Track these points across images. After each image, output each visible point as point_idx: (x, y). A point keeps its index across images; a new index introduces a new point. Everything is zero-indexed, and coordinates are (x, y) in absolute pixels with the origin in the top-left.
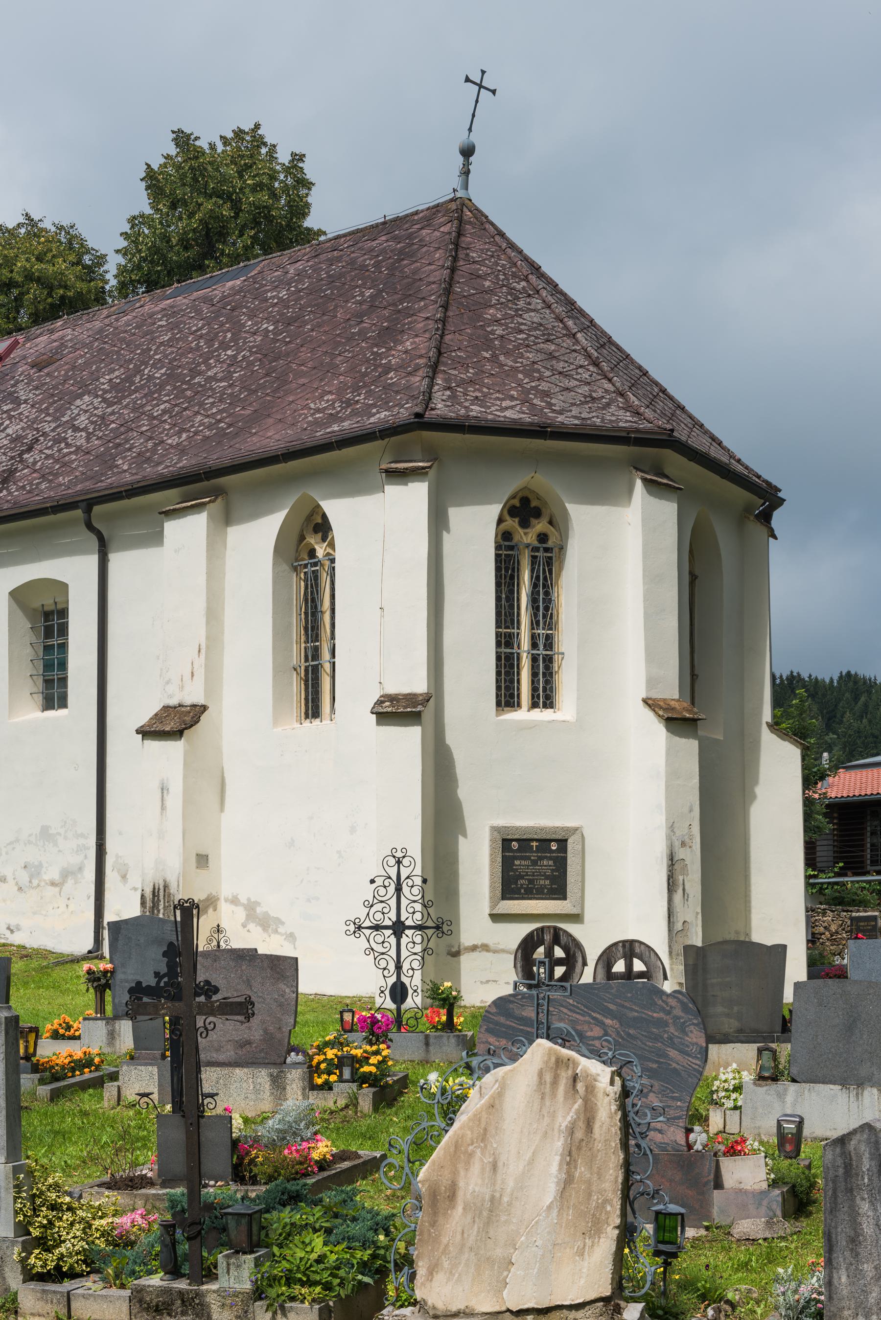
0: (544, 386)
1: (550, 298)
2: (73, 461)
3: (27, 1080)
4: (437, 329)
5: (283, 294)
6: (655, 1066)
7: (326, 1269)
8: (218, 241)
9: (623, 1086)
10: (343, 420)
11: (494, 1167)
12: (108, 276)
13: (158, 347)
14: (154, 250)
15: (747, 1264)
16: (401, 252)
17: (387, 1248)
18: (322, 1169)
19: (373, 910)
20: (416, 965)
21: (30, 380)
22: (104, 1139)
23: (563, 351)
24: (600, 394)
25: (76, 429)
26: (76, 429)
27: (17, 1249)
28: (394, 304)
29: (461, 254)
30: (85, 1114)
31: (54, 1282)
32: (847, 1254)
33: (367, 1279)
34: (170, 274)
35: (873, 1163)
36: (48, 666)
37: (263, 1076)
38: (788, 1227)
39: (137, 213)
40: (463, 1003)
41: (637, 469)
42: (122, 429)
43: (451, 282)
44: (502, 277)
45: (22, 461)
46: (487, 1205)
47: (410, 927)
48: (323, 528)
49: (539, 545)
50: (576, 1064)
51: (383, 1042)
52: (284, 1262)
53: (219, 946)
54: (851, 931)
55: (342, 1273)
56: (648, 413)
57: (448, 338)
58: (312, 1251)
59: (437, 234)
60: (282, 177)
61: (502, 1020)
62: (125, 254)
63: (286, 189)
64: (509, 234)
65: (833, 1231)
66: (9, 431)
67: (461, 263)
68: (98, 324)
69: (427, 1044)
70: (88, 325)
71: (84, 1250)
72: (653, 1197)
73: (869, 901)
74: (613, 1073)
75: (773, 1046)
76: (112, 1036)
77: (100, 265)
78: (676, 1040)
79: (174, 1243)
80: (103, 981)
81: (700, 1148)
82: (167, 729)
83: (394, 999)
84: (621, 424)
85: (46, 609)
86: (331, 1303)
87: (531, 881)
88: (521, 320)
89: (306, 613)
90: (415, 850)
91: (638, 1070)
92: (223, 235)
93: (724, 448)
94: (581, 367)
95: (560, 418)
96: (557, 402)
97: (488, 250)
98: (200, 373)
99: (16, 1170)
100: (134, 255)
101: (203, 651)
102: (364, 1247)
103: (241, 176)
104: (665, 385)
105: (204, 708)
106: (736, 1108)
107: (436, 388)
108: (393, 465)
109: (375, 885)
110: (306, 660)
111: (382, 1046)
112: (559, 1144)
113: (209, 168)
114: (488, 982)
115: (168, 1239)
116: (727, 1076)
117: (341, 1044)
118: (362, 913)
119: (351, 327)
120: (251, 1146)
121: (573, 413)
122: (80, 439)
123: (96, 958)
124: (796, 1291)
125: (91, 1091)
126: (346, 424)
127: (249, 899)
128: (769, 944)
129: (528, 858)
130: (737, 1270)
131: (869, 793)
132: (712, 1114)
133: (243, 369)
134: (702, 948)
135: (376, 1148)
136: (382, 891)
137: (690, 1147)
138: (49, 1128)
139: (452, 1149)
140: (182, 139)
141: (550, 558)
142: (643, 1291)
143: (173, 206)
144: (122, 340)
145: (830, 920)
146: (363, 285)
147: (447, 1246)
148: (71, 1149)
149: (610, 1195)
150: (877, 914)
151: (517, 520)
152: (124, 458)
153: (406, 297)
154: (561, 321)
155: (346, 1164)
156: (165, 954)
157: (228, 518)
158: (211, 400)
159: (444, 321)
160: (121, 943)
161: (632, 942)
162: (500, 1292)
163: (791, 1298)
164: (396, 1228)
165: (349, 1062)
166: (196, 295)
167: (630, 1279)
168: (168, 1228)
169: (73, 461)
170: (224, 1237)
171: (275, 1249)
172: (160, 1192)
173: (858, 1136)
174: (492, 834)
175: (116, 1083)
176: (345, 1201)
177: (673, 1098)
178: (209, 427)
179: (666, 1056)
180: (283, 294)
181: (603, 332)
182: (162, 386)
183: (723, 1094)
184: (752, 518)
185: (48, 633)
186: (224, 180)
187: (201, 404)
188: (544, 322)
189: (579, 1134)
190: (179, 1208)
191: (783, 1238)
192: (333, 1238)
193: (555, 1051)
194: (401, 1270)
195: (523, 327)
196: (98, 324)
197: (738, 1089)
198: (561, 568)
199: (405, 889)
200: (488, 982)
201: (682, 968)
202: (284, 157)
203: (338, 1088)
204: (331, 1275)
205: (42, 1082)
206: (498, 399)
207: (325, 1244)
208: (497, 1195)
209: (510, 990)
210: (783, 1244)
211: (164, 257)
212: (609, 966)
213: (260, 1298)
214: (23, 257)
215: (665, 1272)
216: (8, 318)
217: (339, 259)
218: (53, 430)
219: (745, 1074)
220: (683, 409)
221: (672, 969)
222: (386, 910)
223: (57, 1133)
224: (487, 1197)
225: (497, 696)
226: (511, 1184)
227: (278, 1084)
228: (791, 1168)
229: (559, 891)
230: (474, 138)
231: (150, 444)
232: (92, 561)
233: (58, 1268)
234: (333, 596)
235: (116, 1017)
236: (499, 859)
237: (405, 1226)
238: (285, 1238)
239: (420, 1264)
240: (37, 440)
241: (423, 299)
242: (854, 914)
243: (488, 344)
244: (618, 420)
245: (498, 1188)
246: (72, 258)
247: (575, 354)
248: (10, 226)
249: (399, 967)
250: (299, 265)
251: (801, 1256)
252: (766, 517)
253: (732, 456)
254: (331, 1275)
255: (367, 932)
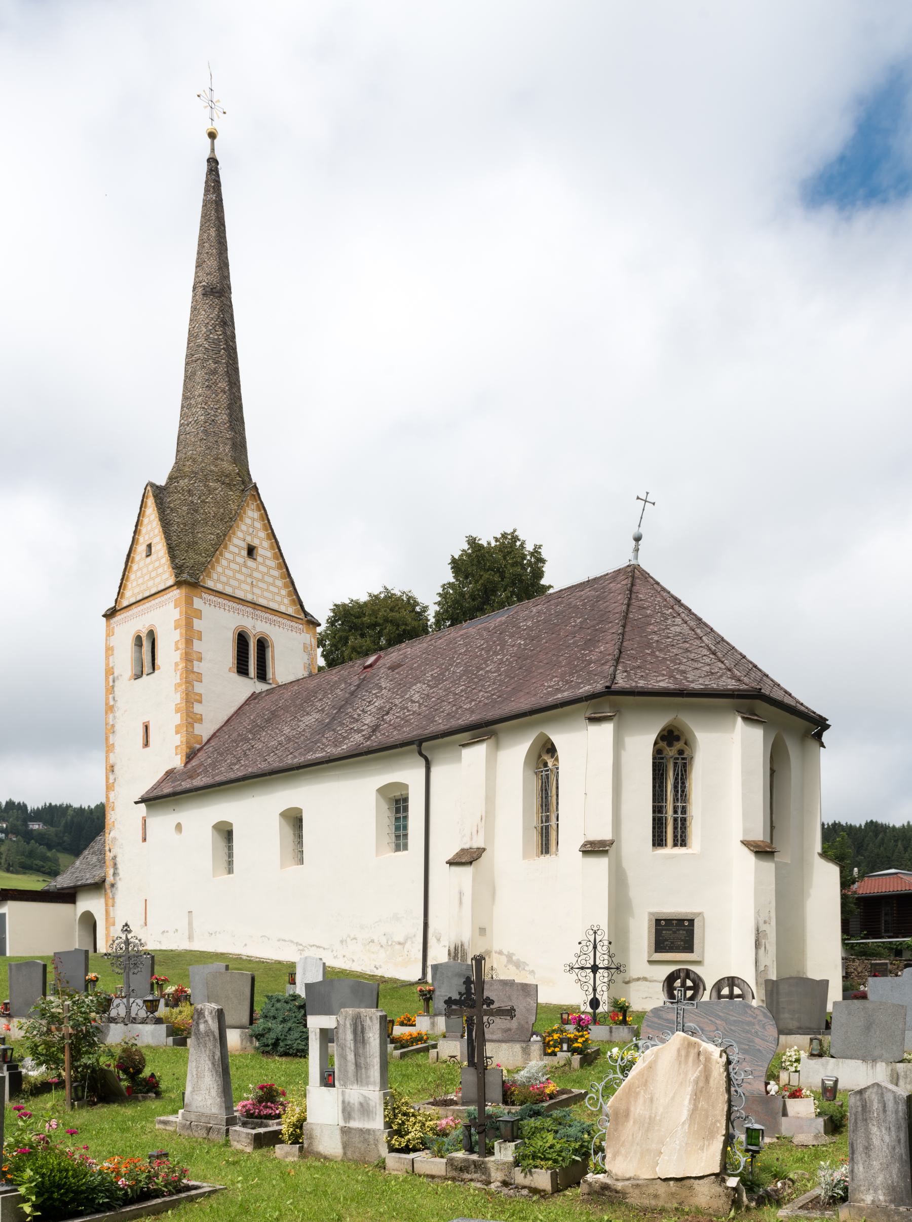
0: (682, 667)
1: (686, 618)
2: (411, 719)
3: (390, 1047)
4: (619, 639)
5: (529, 623)
6: (747, 1047)
7: (555, 1152)
8: (492, 595)
9: (728, 1058)
10: (564, 691)
11: (652, 1100)
12: (429, 617)
13: (459, 656)
14: (456, 602)
15: (802, 1159)
16: (597, 597)
17: (589, 1142)
18: (551, 1098)
19: (580, 958)
20: (605, 988)
21: (387, 675)
22: (430, 1079)
23: (694, 647)
24: (717, 670)
25: (413, 702)
26: (413, 702)
27: (386, 1135)
28: (594, 626)
29: (634, 596)
30: (419, 1066)
31: (405, 1153)
32: (863, 1155)
33: (578, 1158)
34: (464, 614)
35: (880, 1105)
36: (397, 828)
37: (517, 1047)
38: (827, 1139)
39: (446, 582)
40: (631, 1010)
41: (738, 712)
42: (439, 701)
43: (627, 612)
44: (657, 607)
45: (383, 720)
46: (647, 1121)
47: (601, 968)
48: (551, 750)
49: (678, 756)
50: (699, 1046)
51: (586, 1031)
52: (531, 1147)
53: (492, 978)
54: (871, 971)
55: (563, 1154)
56: (746, 680)
57: (625, 644)
58: (547, 1142)
59: (619, 586)
60: (528, 558)
61: (656, 1020)
62: (439, 605)
63: (530, 564)
64: (662, 583)
65: (854, 1142)
66: (376, 704)
67: (634, 601)
68: (425, 645)
69: (611, 1032)
70: (420, 646)
71: (421, 1137)
72: (745, 1120)
73: (883, 954)
74: (721, 1051)
75: (820, 1037)
76: (433, 1024)
77: (425, 611)
78: (759, 1033)
79: (470, 1135)
80: (428, 996)
81: (774, 1093)
82: (463, 861)
83: (592, 1007)
84: (729, 687)
85: (397, 798)
86: (558, 1170)
87: (672, 943)
88: (669, 631)
89: (542, 798)
90: (604, 926)
91: (736, 1050)
92: (494, 591)
93: (793, 697)
94: (705, 655)
95: (692, 685)
96: (690, 676)
97: (649, 593)
98: (482, 669)
99: (385, 1095)
100: (444, 605)
101: (483, 819)
102: (576, 1141)
103: (505, 558)
104: (756, 663)
105: (484, 850)
106: (796, 1071)
107: (618, 671)
108: (593, 715)
109: (581, 945)
110: (542, 822)
111: (585, 1033)
112: (689, 1089)
113: (487, 555)
114: (646, 998)
115: (467, 1133)
116: (791, 1053)
117: (562, 1031)
118: (574, 960)
119: (569, 640)
120: (511, 1085)
121: (700, 682)
122: (415, 707)
123: (423, 983)
124: (832, 1175)
125: (422, 1054)
126: (566, 694)
127: (508, 952)
128: (818, 979)
129: (671, 930)
130: (796, 1162)
131: (883, 891)
132: (781, 1075)
133: (506, 666)
134: (776, 981)
135: (582, 1088)
136: (585, 949)
137: (767, 1093)
138: (399, 1073)
139: (627, 1090)
140: (472, 542)
141: (686, 763)
142: (739, 1171)
143: (466, 577)
144: (439, 653)
145: (857, 965)
146: (576, 616)
147: (624, 1142)
148: (412, 1084)
149: (719, 1118)
150: (887, 961)
151: (665, 743)
152: (439, 717)
153: (601, 622)
154: (693, 630)
155: (565, 1096)
156: (464, 983)
157: (497, 746)
158: (488, 683)
159: (623, 634)
160: (438, 975)
161: (733, 978)
162: (655, 1168)
163: (829, 1179)
164: (594, 1131)
165: (566, 1041)
166: (479, 627)
167: (731, 1164)
168: (468, 1127)
169: (411, 719)
170: (498, 1133)
171: (526, 1140)
172: (461, 1108)
173: (870, 1090)
174: (649, 916)
175: (436, 1050)
176: (565, 1116)
177: (758, 1065)
178: (487, 698)
179: (753, 1041)
180: (529, 623)
181: (718, 635)
182: (460, 678)
183: (789, 1063)
184: (810, 736)
185: (397, 811)
186: (496, 561)
187: (483, 686)
188: (682, 631)
189: (701, 1084)
190: (473, 1117)
191: (824, 1145)
192: (558, 1135)
193: (687, 1039)
194: (597, 1154)
195: (670, 635)
196: (425, 645)
197: (798, 1061)
198: (691, 769)
199: (599, 947)
200: (646, 998)
201: (764, 991)
202: (529, 547)
203: (560, 1054)
204: (557, 1155)
205: (396, 1048)
206: (655, 676)
207: (554, 1138)
208: (653, 1115)
209: (662, 1004)
210: (824, 1149)
211: (462, 606)
212: (719, 991)
213: (518, 1166)
214: (383, 610)
215: (752, 1161)
216: (374, 642)
217: (561, 603)
218: (400, 703)
219: (802, 1052)
220: (767, 676)
221: (757, 992)
222: (587, 959)
223: (404, 1075)
224: (647, 1116)
225: (653, 840)
226: (661, 1110)
227: (526, 1052)
228: (831, 1107)
229: (689, 948)
230: (642, 530)
231: (454, 708)
232: (423, 771)
233: (407, 1146)
234: (557, 788)
235: (436, 1015)
236: (654, 931)
237: (599, 1130)
238: (532, 1135)
239: (608, 1151)
240: (391, 708)
241: (611, 622)
242: (873, 962)
243: (649, 645)
244: (727, 685)
245: (653, 1111)
246: (410, 609)
247: (701, 649)
248: (376, 594)
249: (595, 990)
250: (539, 607)
251: (836, 1156)
252: (818, 736)
253: (798, 702)
254: (557, 1155)
255: (577, 970)
